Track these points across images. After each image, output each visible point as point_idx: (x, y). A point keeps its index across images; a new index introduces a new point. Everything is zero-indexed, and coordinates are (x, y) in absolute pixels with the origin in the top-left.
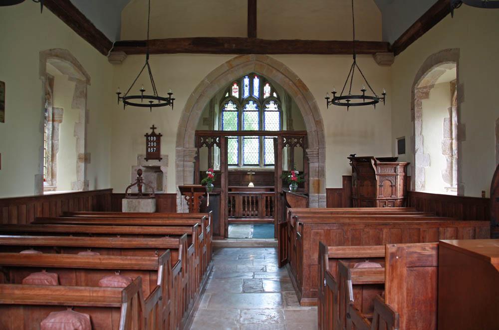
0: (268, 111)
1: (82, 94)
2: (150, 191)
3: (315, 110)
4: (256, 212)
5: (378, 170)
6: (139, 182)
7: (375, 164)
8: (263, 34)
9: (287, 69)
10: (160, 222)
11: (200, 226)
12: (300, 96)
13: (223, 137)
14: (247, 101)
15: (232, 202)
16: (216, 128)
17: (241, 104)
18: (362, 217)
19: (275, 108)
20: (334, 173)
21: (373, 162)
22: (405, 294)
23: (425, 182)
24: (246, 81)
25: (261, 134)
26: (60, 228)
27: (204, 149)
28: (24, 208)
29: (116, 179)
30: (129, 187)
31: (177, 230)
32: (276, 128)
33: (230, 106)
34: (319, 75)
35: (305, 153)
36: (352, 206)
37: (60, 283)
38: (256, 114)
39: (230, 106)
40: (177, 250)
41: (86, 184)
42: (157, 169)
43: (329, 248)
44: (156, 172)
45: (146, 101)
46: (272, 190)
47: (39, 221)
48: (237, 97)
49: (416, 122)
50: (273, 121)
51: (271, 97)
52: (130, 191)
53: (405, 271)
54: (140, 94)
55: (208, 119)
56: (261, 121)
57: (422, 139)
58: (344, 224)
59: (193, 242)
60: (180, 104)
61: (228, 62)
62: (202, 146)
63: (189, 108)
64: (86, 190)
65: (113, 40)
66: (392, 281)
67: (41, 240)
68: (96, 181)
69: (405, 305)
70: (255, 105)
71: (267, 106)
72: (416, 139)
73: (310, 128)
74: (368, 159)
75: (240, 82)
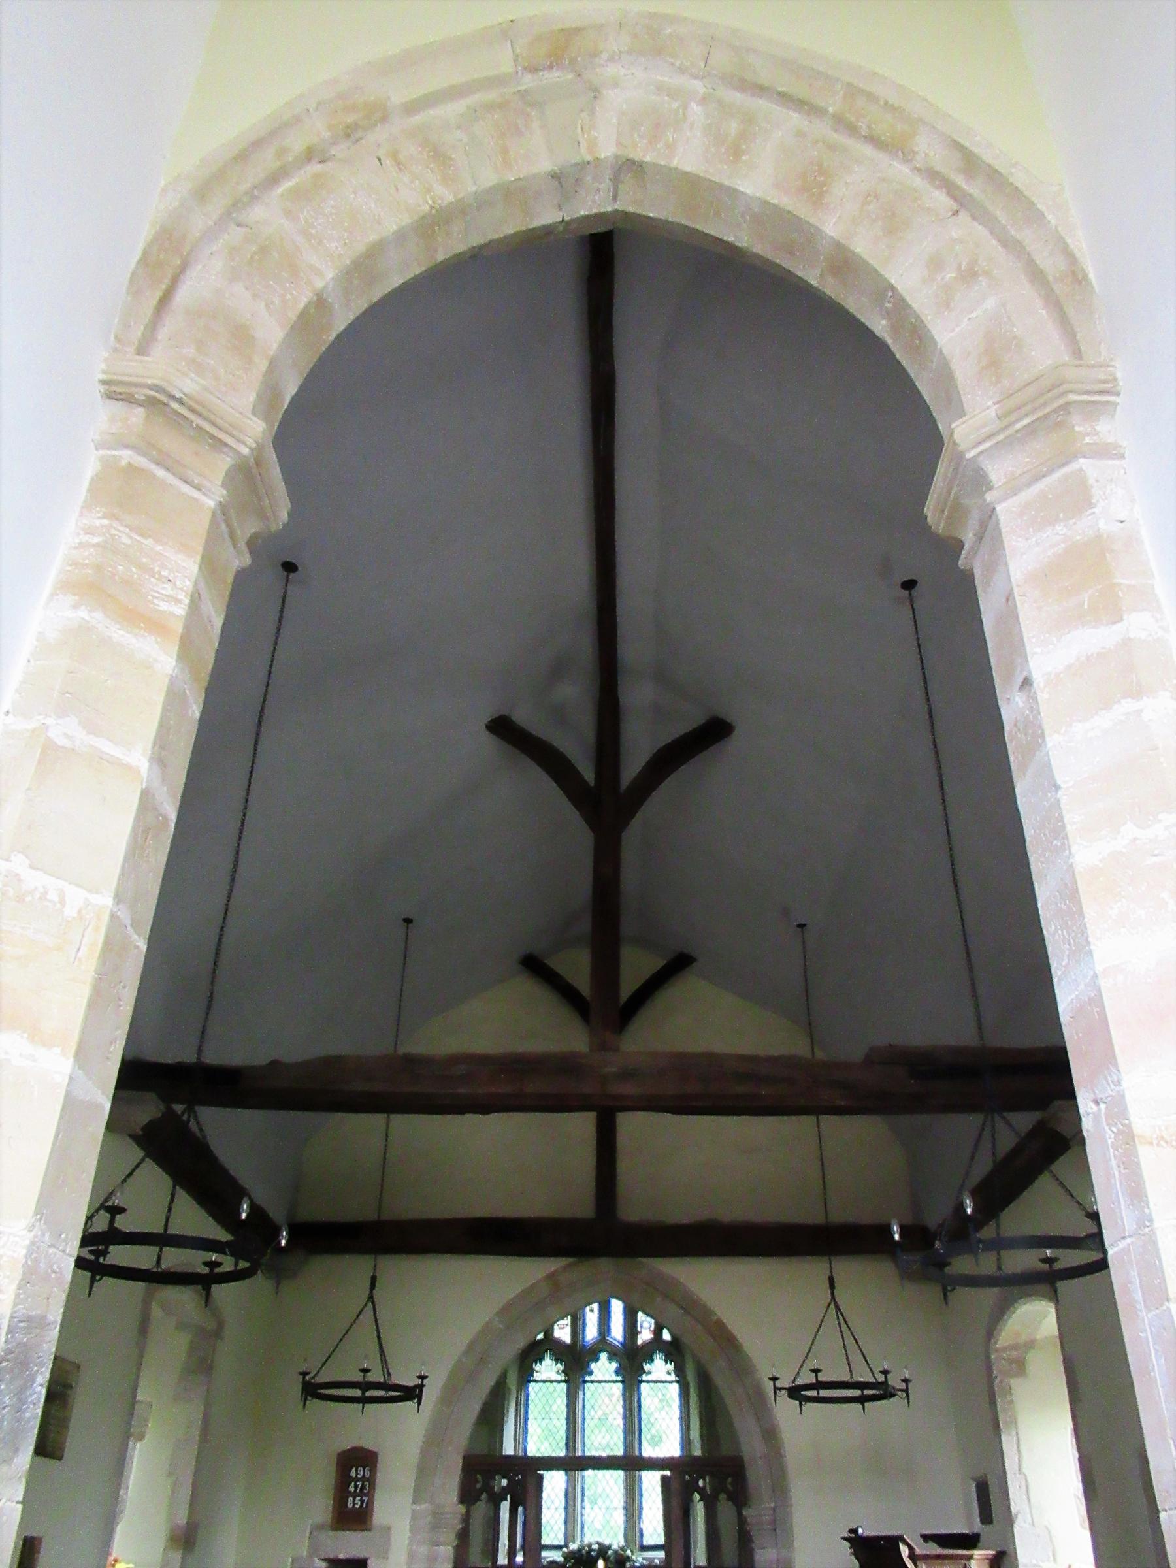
0: (648, 1382)
7: (913, 1556)
8: (635, 1206)
14: (593, 1353)
17: (576, 1361)
19: (669, 1373)
21: (904, 1551)
25: (631, 1463)
27: (481, 1508)
32: (671, 1448)
33: (548, 1368)
34: (771, 1314)
35: (742, 1522)
38: (618, 1389)
39: (548, 1368)
49: (1003, 1438)
50: (666, 1431)
51: (657, 1343)
54: (358, 1377)
55: (491, 1417)
57: (1023, 1483)
61: (551, 1276)
62: (478, 1499)
70: (614, 1365)
71: (646, 1367)
72: (1010, 1486)
73: (751, 1446)
74: (893, 1542)
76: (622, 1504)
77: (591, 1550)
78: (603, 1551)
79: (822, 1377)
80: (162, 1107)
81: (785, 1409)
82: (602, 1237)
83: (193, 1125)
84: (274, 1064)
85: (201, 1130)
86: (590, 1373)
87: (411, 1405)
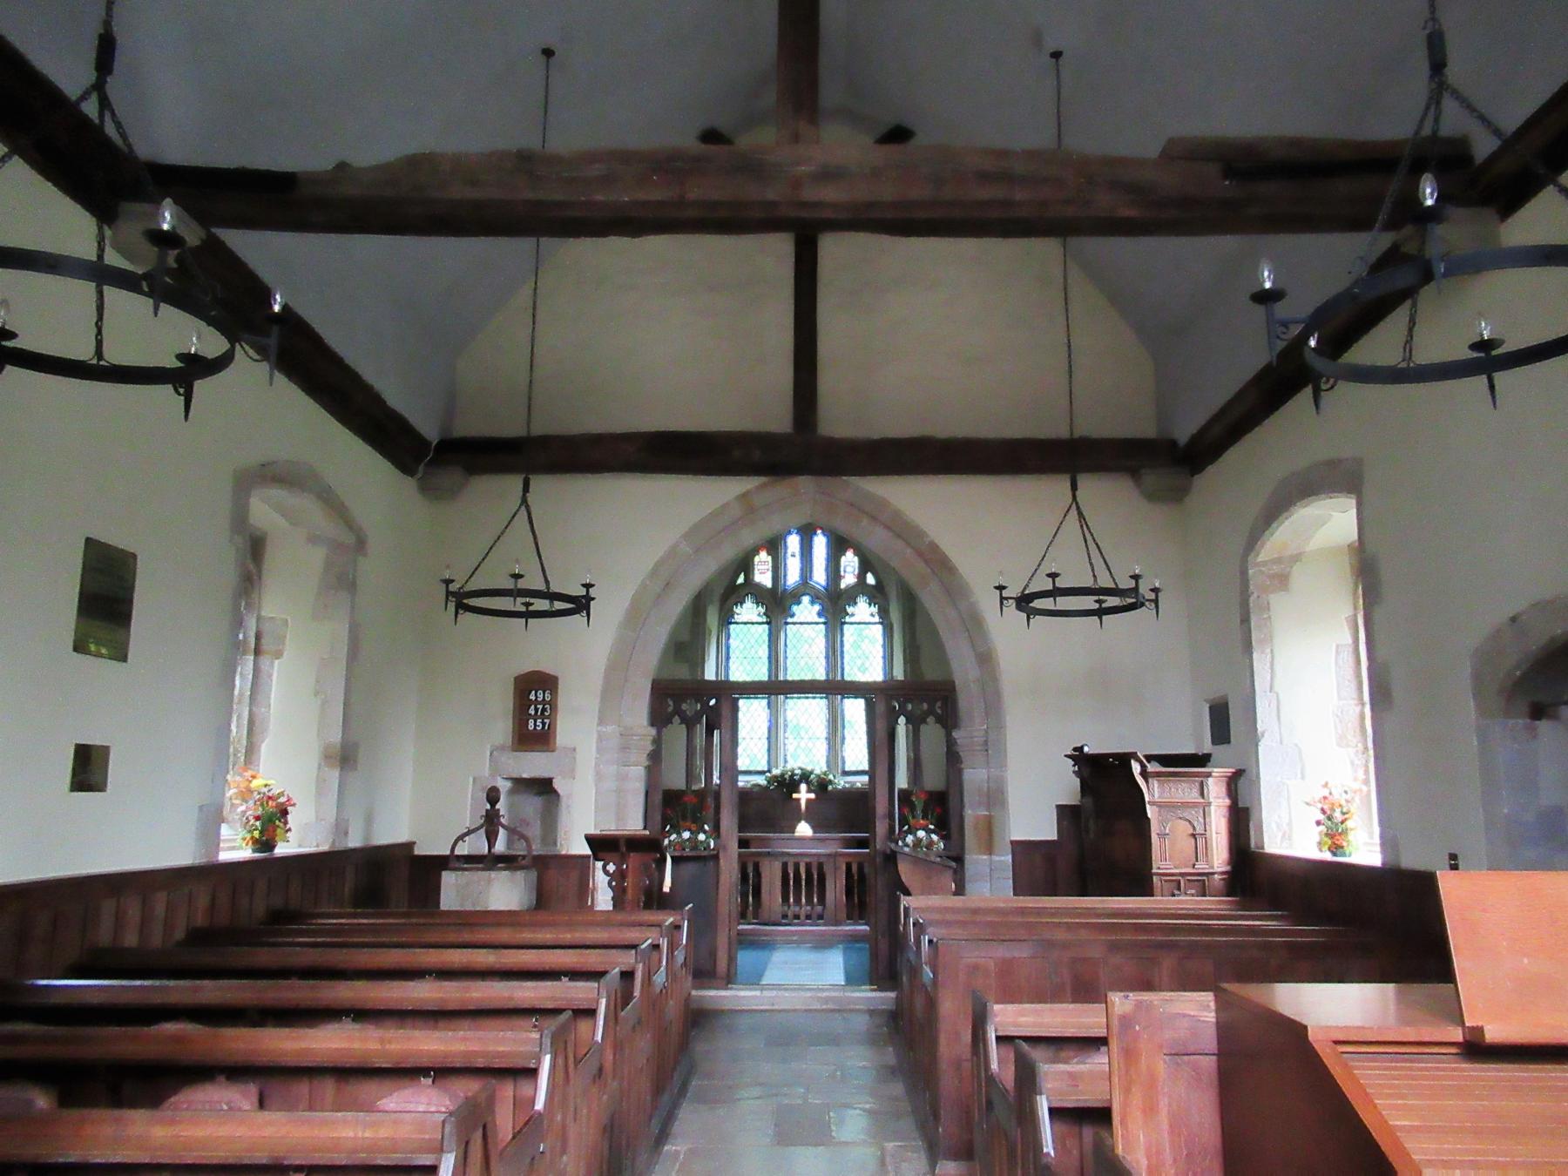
1: (342, 580)
2: (520, 849)
3: (974, 625)
4: (819, 908)
5: (1152, 792)
6: (491, 822)
7: (1144, 774)
8: (839, 418)
9: (897, 514)
10: (547, 936)
11: (656, 947)
12: (934, 586)
13: (731, 692)
14: (795, 596)
15: (750, 881)
16: (710, 674)
17: (777, 604)
18: (1107, 927)
20: (1030, 797)
21: (1136, 768)
22: (1165, 1126)
23: (1290, 824)
24: (793, 542)
25: (834, 688)
26: (264, 957)
27: (677, 731)
28: (160, 902)
29: (420, 806)
30: (461, 838)
31: (592, 959)
32: (873, 672)
33: (749, 611)
34: (986, 533)
35: (951, 744)
36: (1083, 893)
37: (262, 1104)
39: (749, 611)
40: (591, 1013)
41: (341, 828)
42: (543, 787)
43: (997, 1007)
44: (540, 794)
45: (518, 605)
46: (862, 843)
47: (199, 937)
48: (769, 584)
49: (1255, 655)
50: (867, 651)
52: (463, 849)
53: (1161, 1066)
54: (509, 584)
55: (689, 641)
56: (834, 652)
58: (1050, 944)
59: (637, 993)
60: (609, 610)
63: (635, 617)
64: (339, 847)
65: (429, 430)
66: (1127, 1091)
67: (211, 991)
68: (369, 820)
69: (1168, 1157)
70: (817, 607)
71: (850, 610)
73: (964, 670)
74: (1124, 759)
75: (774, 546)
76: (825, 735)
77: (793, 775)
78: (805, 776)
79: (1060, 583)
80: (202, 234)
81: (1007, 631)
82: (798, 451)
83: (110, 129)
84: (342, 166)
85: (123, 136)
86: (793, 616)
87: (579, 619)
